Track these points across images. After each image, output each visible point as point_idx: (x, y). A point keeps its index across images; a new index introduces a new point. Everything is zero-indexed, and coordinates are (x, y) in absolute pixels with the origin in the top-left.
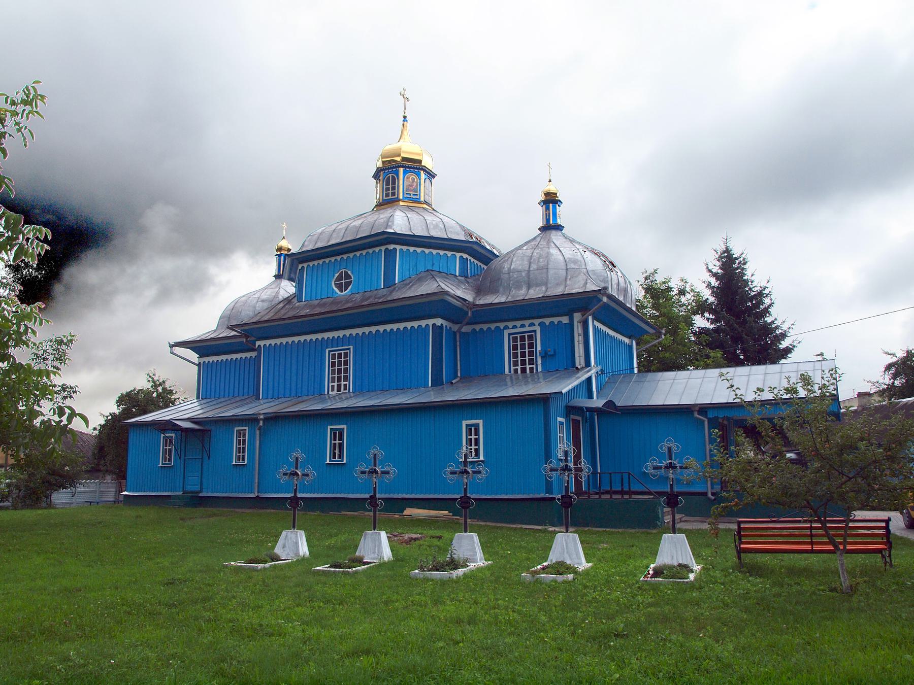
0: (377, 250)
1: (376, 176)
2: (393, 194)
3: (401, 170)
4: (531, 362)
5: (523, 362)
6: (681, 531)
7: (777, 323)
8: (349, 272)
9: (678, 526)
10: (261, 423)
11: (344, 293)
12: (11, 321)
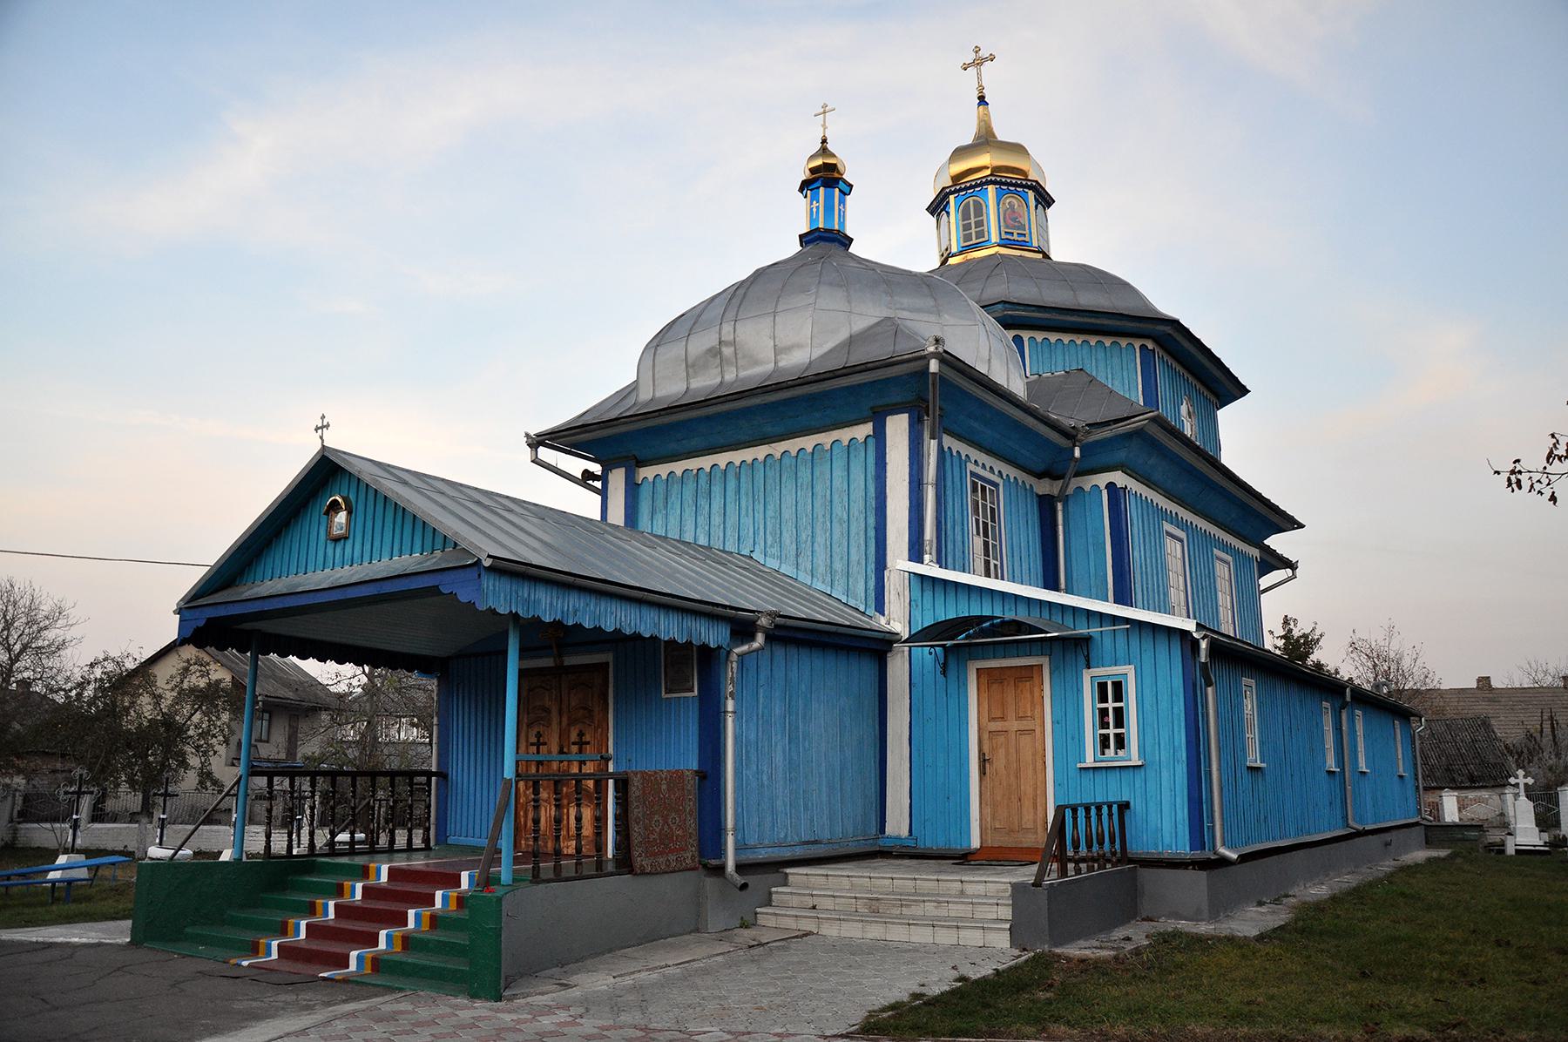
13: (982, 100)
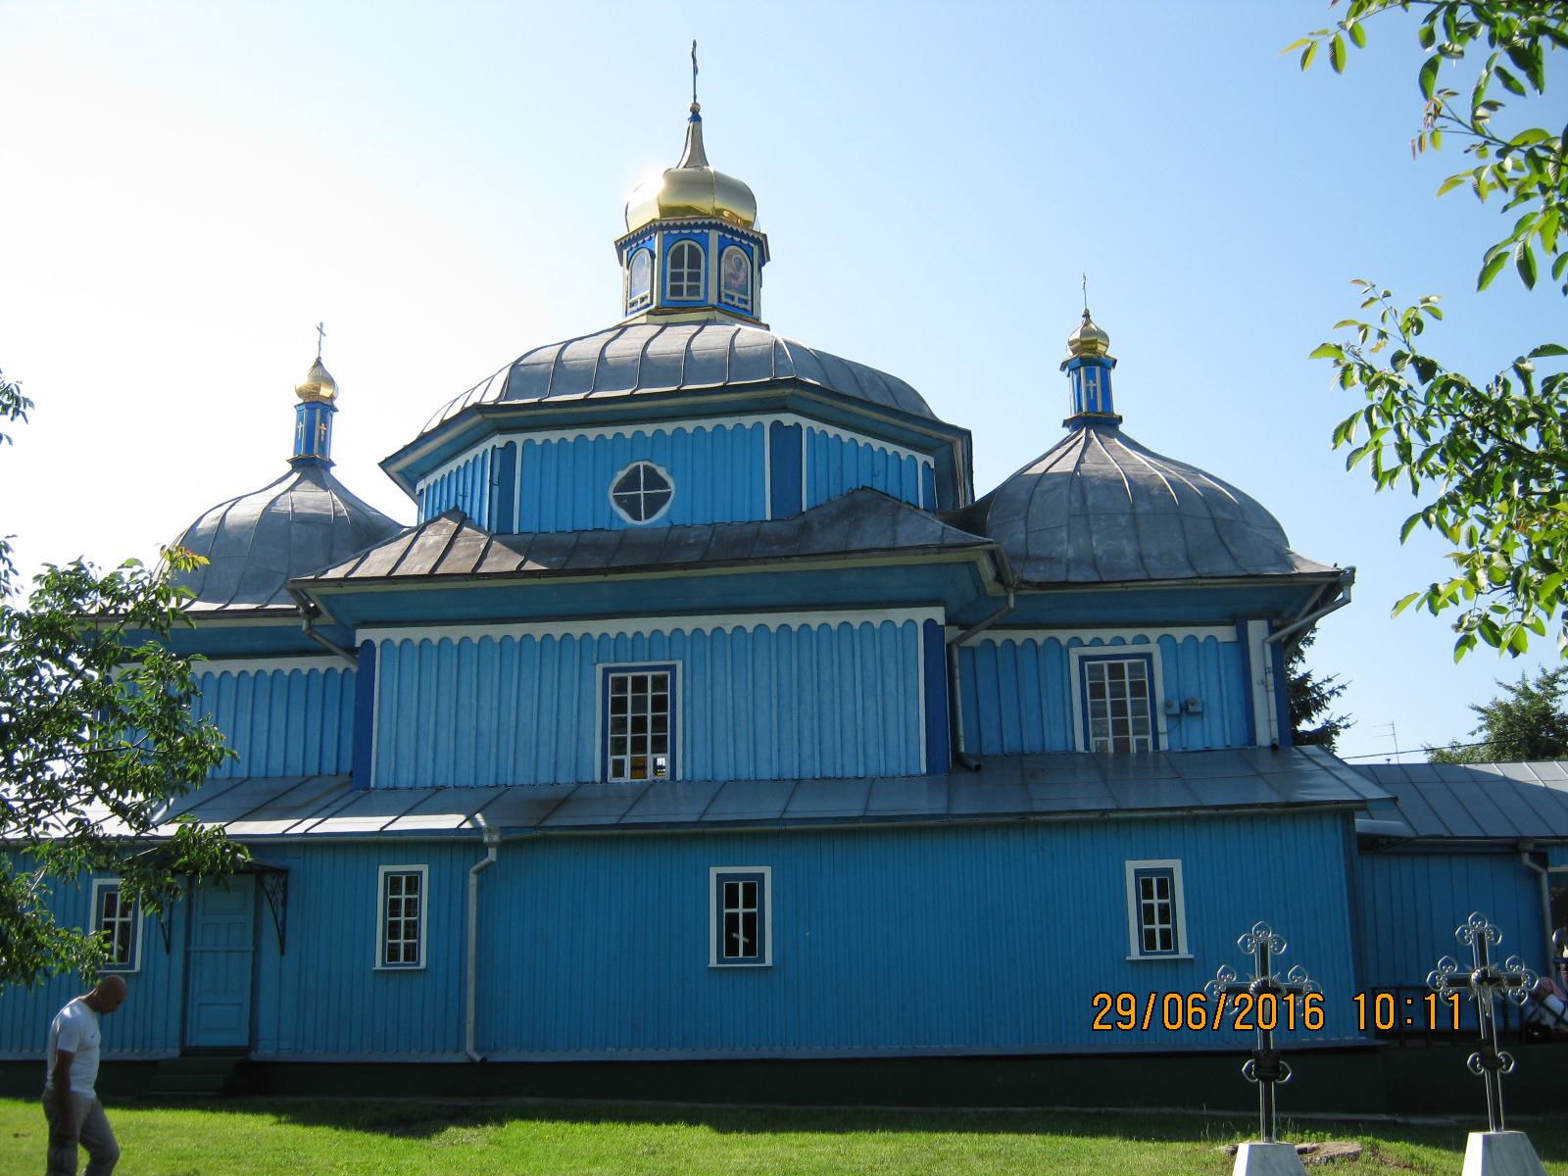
0: (748, 421)
2: (694, 290)
3: (714, 236)
7: (1316, 679)
8: (662, 472)
10: (492, 855)
11: (644, 522)
12: (1510, 415)
13: (696, 117)
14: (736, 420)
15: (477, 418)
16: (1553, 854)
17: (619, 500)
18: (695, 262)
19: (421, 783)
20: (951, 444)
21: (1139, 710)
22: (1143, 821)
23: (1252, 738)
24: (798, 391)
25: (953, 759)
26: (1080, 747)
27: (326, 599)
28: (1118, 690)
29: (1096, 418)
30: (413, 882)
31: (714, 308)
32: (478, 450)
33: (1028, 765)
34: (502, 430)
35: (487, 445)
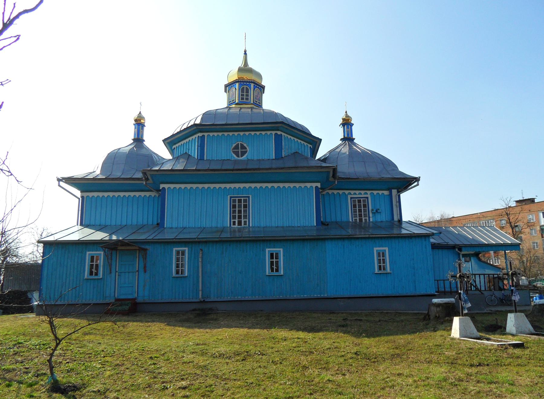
0: (269, 133)
1: (228, 87)
2: (247, 99)
3: (252, 85)
4: (245, 217)
5: (240, 217)
6: (521, 311)
8: (245, 145)
9: (518, 309)
13: (245, 53)
14: (265, 132)
15: (195, 128)
16: (463, 249)
17: (234, 152)
18: (247, 92)
19: (179, 226)
20: (317, 142)
21: (365, 211)
22: (378, 237)
23: (393, 219)
24: (283, 125)
25: (321, 223)
26: (351, 220)
27: (152, 176)
28: (360, 206)
29: (348, 139)
30: (183, 253)
31: (252, 104)
32: (194, 137)
33: (339, 225)
34: (201, 131)
35: (197, 136)
